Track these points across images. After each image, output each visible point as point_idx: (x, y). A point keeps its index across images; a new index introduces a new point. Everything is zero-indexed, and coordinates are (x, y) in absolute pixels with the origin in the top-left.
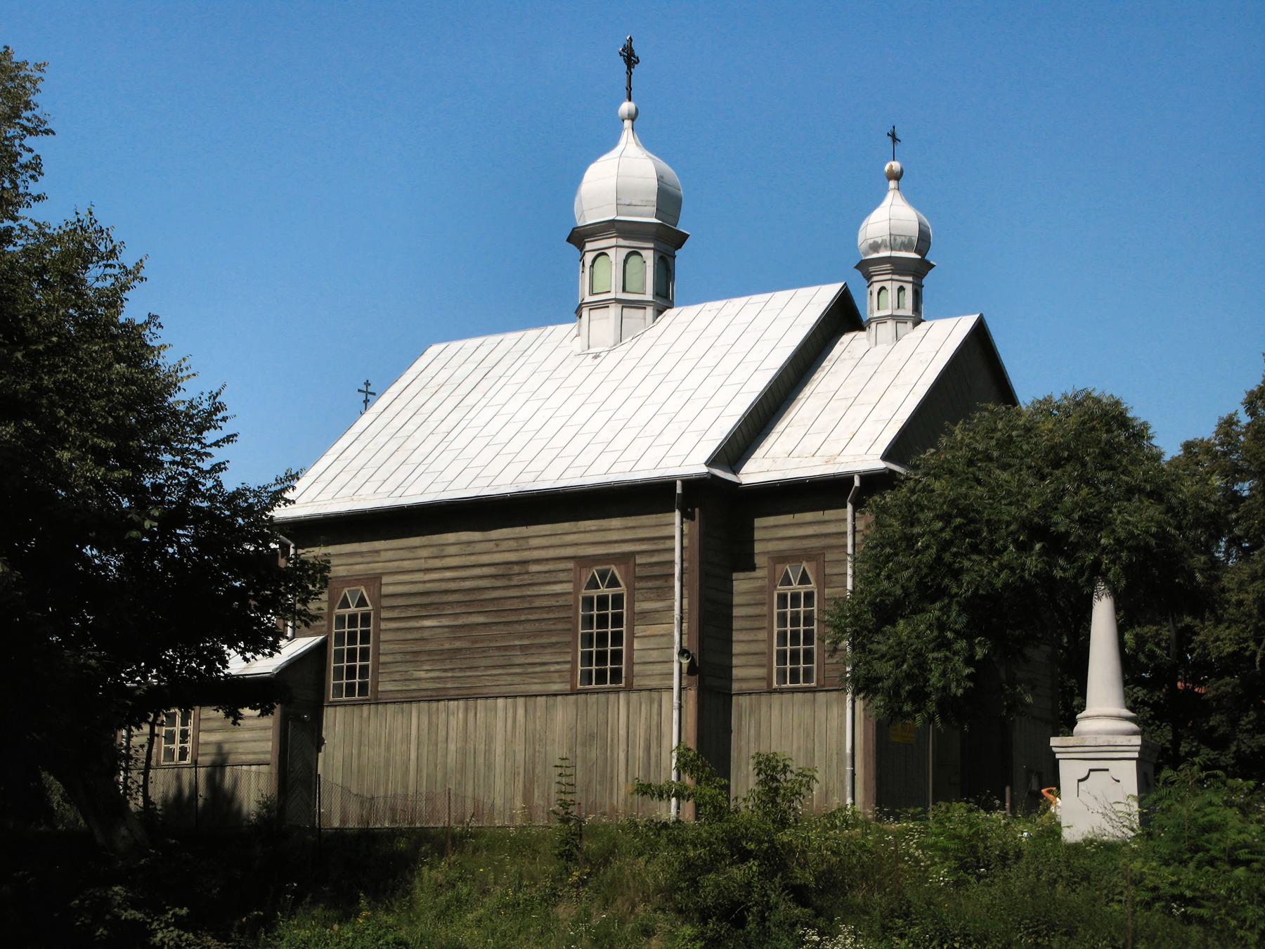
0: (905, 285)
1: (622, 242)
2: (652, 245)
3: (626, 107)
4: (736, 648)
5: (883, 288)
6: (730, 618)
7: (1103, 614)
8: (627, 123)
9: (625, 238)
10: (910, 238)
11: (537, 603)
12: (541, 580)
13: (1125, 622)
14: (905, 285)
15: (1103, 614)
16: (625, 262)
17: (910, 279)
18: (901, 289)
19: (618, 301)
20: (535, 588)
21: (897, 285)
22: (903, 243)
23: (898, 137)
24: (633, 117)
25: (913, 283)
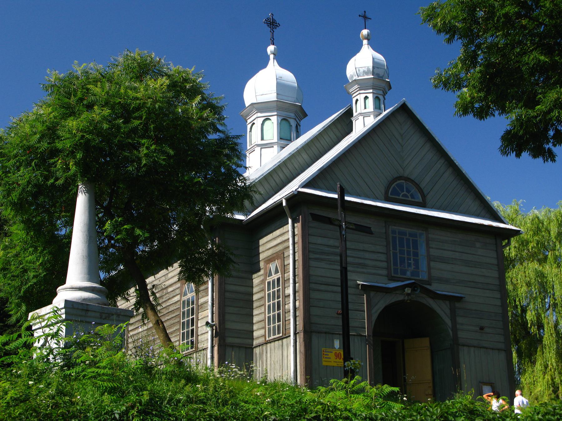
0: (368, 95)
1: (259, 115)
2: (276, 113)
3: (365, 32)
4: (255, 319)
5: (357, 100)
6: (252, 302)
7: (82, 201)
8: (365, 42)
9: (261, 112)
10: (368, 68)
11: (171, 309)
12: (171, 296)
13: (95, 203)
14: (368, 95)
15: (82, 201)
16: (263, 124)
17: (371, 91)
18: (366, 98)
19: (258, 145)
20: (170, 301)
21: (364, 95)
22: (364, 71)
23: (368, 15)
24: (368, 38)
25: (373, 93)
